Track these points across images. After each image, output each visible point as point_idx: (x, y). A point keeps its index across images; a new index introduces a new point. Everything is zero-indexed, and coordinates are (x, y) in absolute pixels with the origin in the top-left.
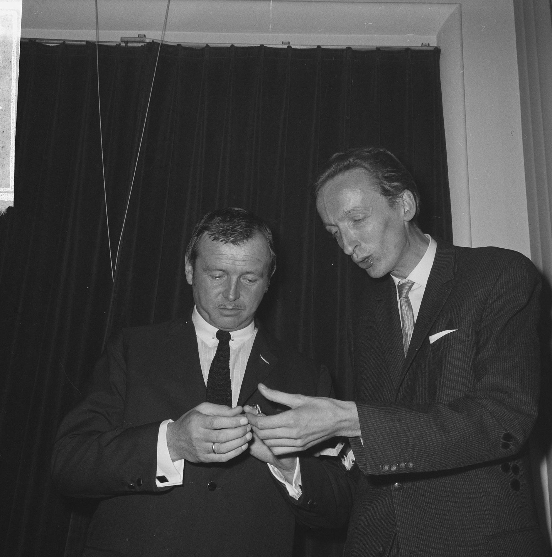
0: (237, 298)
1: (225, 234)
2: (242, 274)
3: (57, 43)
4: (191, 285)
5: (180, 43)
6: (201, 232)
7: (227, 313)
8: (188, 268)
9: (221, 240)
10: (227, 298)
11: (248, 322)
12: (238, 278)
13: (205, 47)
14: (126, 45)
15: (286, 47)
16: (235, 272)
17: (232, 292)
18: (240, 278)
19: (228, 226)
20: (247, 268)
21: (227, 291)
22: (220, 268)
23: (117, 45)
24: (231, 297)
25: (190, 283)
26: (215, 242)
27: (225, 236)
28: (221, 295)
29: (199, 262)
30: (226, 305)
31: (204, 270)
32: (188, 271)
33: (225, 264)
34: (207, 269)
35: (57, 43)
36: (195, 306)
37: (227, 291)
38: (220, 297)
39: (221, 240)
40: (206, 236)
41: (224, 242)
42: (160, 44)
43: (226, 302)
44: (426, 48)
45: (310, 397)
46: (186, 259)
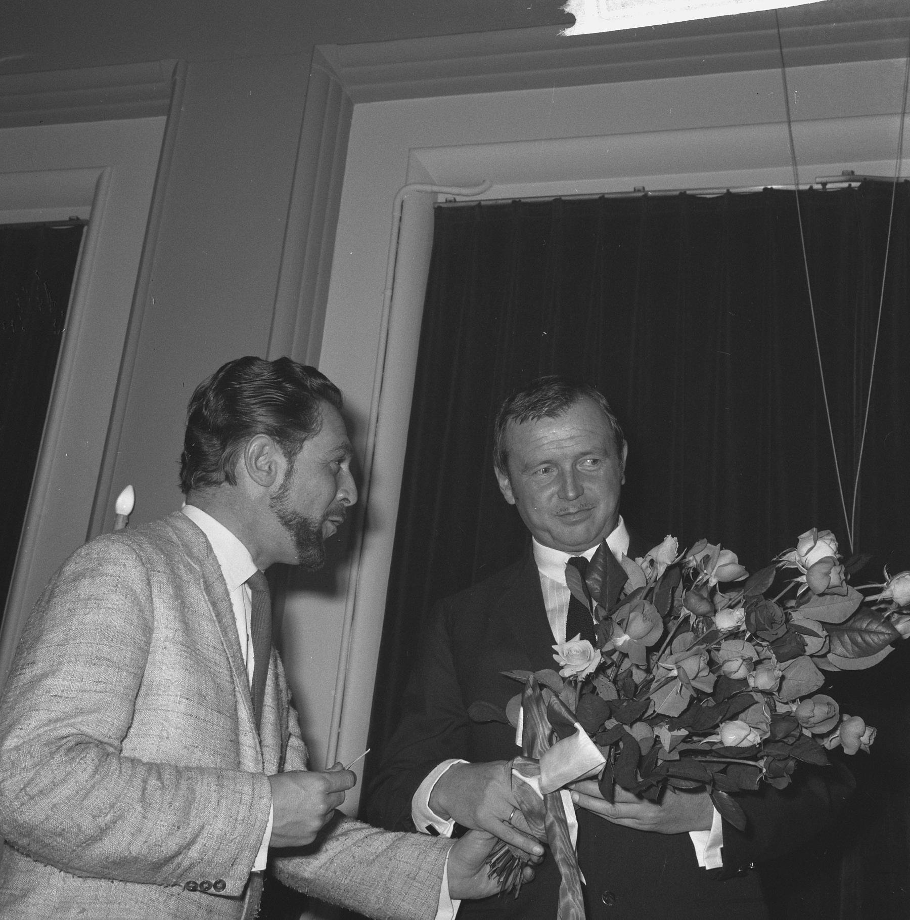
0: (580, 493)
1: (535, 407)
2: (578, 458)
3: (713, 194)
4: (514, 506)
5: (352, 592)
6: (503, 421)
7: (573, 519)
8: (503, 482)
9: (531, 417)
10: (567, 499)
11: (608, 528)
12: (572, 465)
13: (725, 194)
14: (823, 189)
15: (640, 194)
16: (565, 456)
17: (570, 487)
18: (576, 465)
19: (536, 397)
20: (579, 449)
21: (563, 489)
22: (544, 459)
23: (681, 193)
24: (571, 494)
25: (512, 501)
26: (525, 424)
27: (536, 410)
28: (556, 496)
29: (513, 464)
30: (567, 508)
31: (523, 471)
32: (504, 488)
33: (550, 452)
34: (526, 468)
35: (713, 194)
36: (533, 537)
37: (563, 489)
38: (555, 499)
39: (531, 417)
40: (512, 424)
41: (535, 419)
42: (797, 193)
43: (566, 505)
44: (451, 205)
45: (433, 232)
46: (497, 470)
